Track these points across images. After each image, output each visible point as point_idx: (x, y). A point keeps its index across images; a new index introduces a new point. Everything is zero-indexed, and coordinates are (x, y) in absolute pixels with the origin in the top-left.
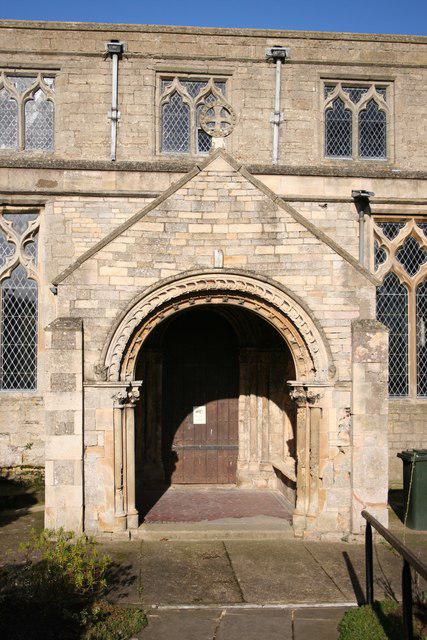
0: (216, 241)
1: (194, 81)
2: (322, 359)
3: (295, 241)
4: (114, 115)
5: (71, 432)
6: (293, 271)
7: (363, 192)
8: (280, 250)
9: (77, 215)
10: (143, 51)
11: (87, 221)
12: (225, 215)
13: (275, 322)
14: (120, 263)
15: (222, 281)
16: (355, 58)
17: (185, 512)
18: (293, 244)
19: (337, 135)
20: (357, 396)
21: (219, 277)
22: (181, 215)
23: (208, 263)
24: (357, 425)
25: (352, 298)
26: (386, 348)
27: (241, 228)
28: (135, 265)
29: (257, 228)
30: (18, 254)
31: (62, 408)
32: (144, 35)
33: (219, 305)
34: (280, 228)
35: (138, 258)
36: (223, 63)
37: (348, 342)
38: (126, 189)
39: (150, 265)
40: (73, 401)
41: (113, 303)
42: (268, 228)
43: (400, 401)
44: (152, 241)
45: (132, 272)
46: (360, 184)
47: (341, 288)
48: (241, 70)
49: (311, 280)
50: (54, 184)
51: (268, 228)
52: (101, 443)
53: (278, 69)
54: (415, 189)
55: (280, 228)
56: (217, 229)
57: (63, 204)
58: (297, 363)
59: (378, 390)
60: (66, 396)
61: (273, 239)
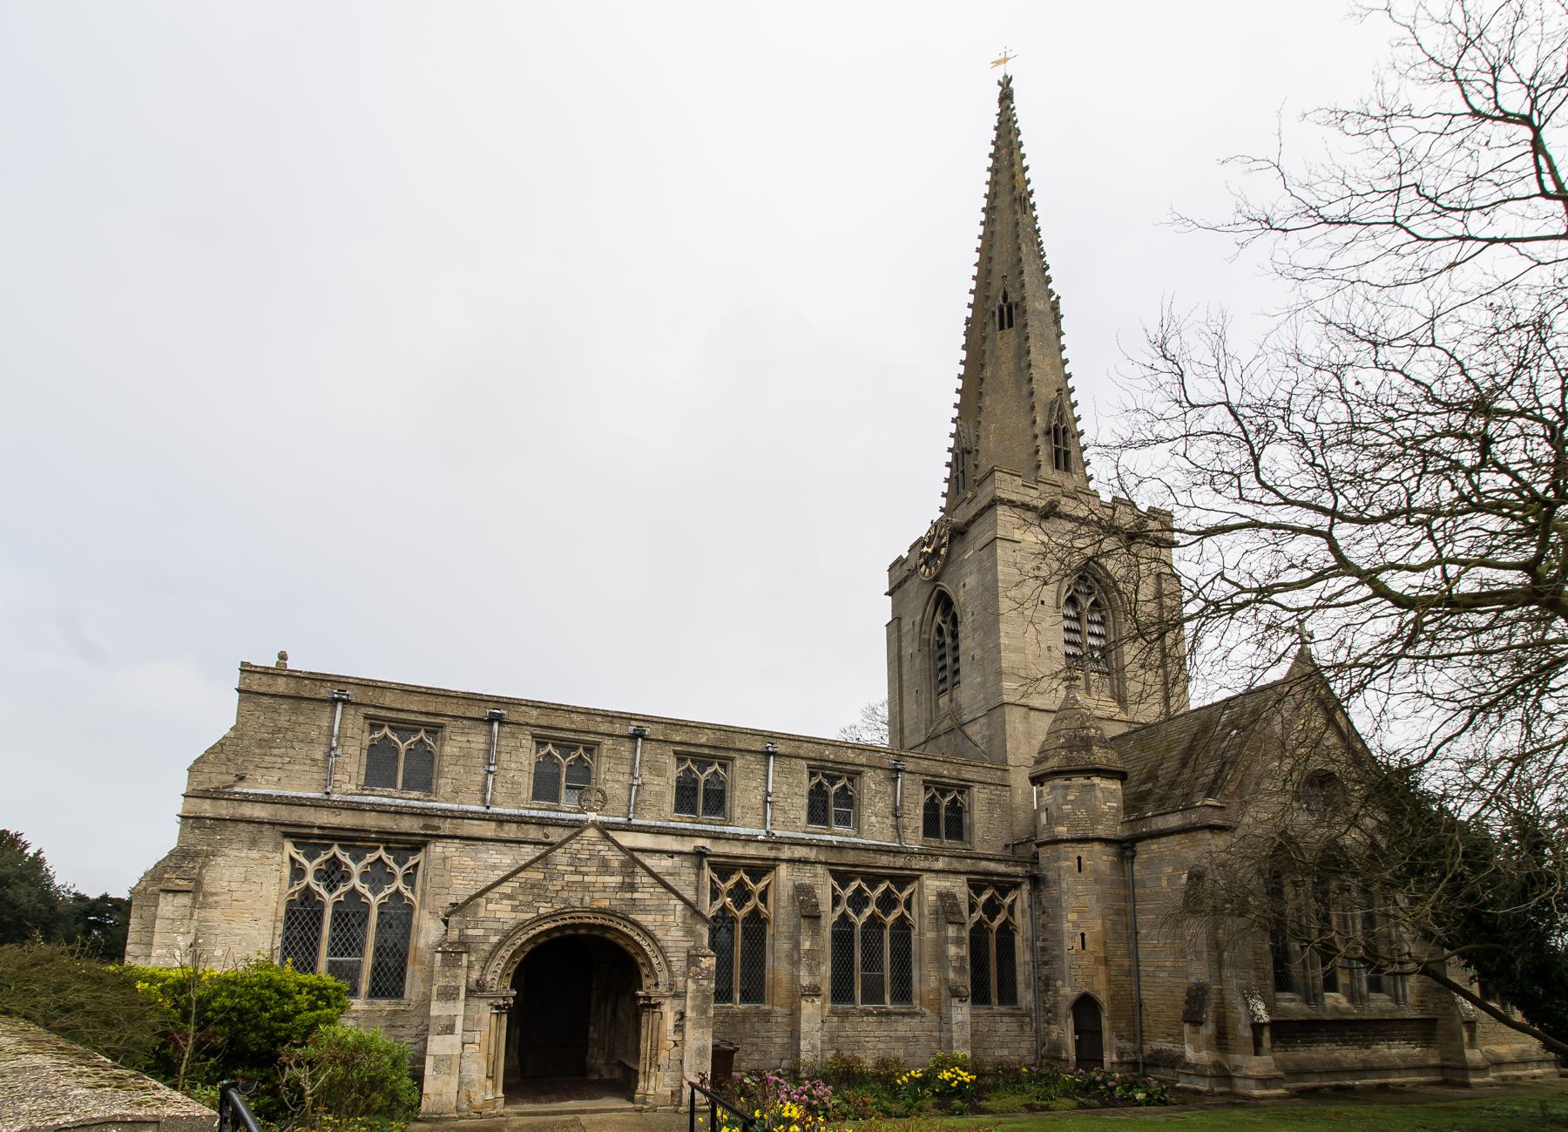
0: (586, 887)
1: (566, 746)
2: (663, 977)
3: (647, 890)
4: (492, 768)
5: (452, 1033)
6: (646, 911)
7: (703, 847)
8: (636, 895)
9: (458, 854)
10: (522, 720)
11: (466, 859)
12: (595, 869)
13: (629, 948)
14: (505, 902)
15: (581, 918)
16: (703, 740)
17: (1062, 831)
18: (647, 892)
19: (686, 797)
20: (689, 1003)
21: (587, 915)
22: (559, 867)
23: (578, 904)
24: (688, 1025)
25: (689, 932)
26: (713, 968)
27: (608, 879)
28: (517, 903)
29: (619, 879)
30: (399, 883)
31: (445, 1013)
32: (523, 708)
33: (584, 935)
34: (638, 880)
35: (521, 898)
36: (593, 736)
37: (685, 963)
38: (503, 835)
39: (530, 904)
40: (458, 1008)
41: (496, 932)
42: (627, 880)
43: (983, 1010)
44: (533, 886)
45: (514, 909)
46: (700, 842)
47: (681, 925)
48: (608, 743)
49: (659, 918)
50: (438, 828)
51: (627, 880)
52: (477, 1041)
53: (639, 744)
54: (743, 847)
55: (638, 880)
56: (587, 879)
57: (444, 845)
58: (643, 977)
59: (707, 997)
60: (451, 1004)
61: (632, 888)
